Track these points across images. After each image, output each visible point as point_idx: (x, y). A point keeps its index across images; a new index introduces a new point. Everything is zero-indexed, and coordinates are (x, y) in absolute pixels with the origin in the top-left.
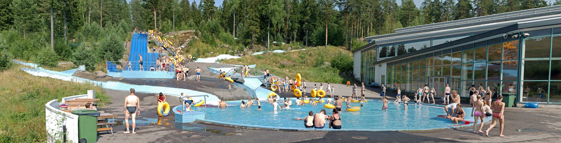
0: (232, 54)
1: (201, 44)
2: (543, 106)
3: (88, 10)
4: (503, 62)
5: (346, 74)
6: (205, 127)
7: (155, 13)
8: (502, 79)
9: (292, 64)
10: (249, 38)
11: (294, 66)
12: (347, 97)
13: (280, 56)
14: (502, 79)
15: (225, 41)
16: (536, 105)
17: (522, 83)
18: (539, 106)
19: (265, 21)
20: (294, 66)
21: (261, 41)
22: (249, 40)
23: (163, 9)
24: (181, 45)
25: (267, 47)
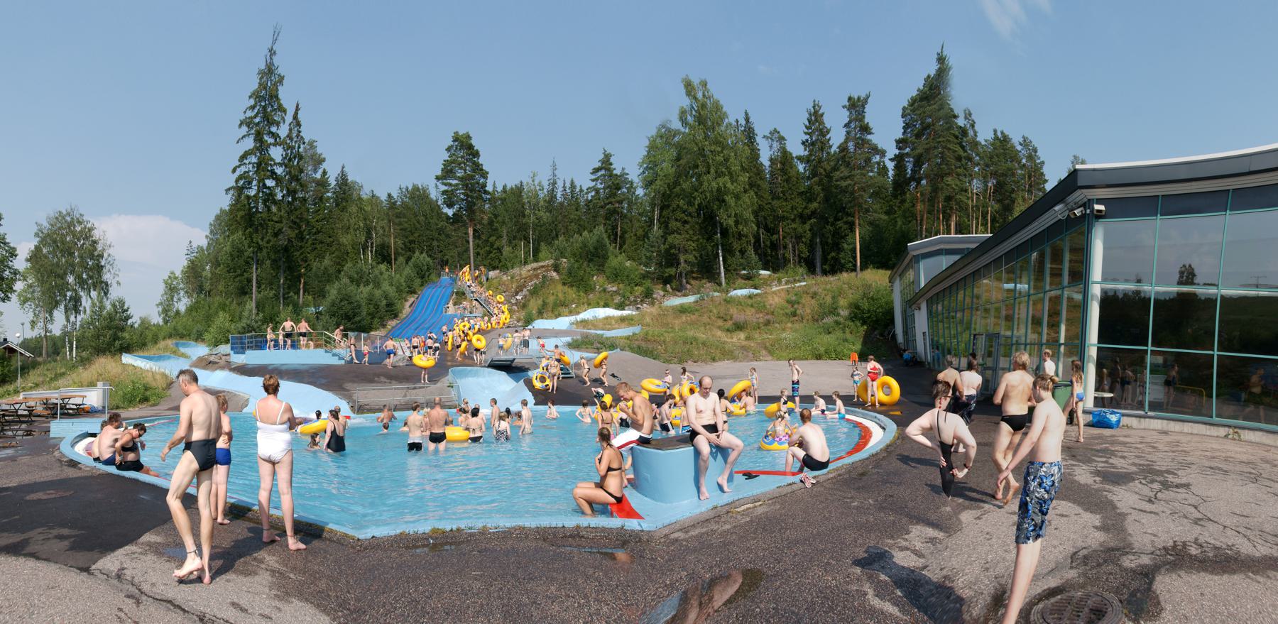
0: (620, 307)
1: (560, 287)
2: (1133, 422)
3: (369, 236)
4: (1049, 295)
5: (882, 335)
6: (29, 549)
7: (471, 231)
8: (1062, 340)
9: (761, 318)
10: (671, 265)
11: (768, 323)
12: (775, 399)
13: (739, 303)
14: (1062, 340)
15: (616, 276)
16: (1114, 418)
17: (1093, 352)
18: (1125, 421)
19: (708, 221)
20: (768, 323)
21: (706, 270)
22: (672, 271)
23: (485, 222)
25: (720, 284)
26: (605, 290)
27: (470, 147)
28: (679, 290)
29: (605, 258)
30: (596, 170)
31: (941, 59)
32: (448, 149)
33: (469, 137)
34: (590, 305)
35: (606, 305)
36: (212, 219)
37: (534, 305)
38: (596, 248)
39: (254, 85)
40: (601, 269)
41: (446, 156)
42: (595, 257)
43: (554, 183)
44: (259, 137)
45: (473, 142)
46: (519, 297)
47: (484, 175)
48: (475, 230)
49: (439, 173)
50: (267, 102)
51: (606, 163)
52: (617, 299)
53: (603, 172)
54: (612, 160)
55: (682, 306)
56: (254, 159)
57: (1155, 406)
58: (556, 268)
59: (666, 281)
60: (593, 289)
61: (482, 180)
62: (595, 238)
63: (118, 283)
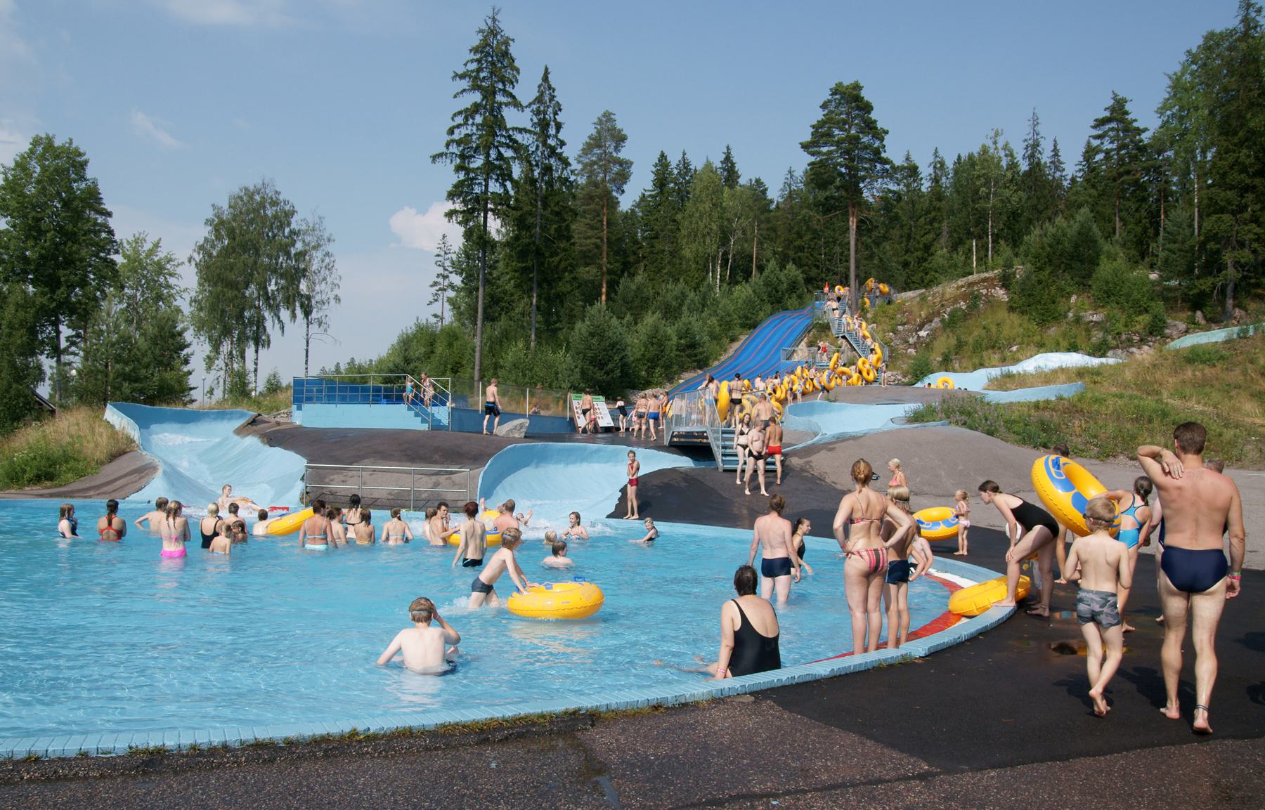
7: (853, 223)
15: (1108, 295)
22: (1205, 284)
24: (921, 327)
26: (1078, 320)
27: (858, 99)
28: (1215, 321)
29: (1094, 262)
30: (1100, 123)
31: (728, 148)
32: (824, 106)
33: (857, 87)
34: (1042, 347)
35: (1073, 348)
36: (1195, 42)
37: (944, 343)
38: (1077, 246)
39: (476, 40)
40: (1083, 284)
41: (819, 115)
42: (1076, 261)
43: (1036, 145)
44: (489, 93)
45: (863, 93)
46: (923, 333)
47: (880, 135)
48: (861, 223)
49: (807, 138)
50: (493, 63)
51: (1118, 111)
52: (1097, 336)
53: (1114, 125)
54: (1128, 107)
55: (1194, 349)
56: (479, 119)
57: (1254, 463)
58: (1005, 281)
59: (1196, 302)
60: (1057, 318)
61: (877, 144)
62: (1076, 227)
63: (337, 299)
